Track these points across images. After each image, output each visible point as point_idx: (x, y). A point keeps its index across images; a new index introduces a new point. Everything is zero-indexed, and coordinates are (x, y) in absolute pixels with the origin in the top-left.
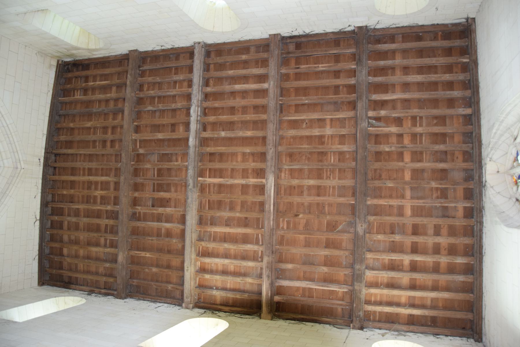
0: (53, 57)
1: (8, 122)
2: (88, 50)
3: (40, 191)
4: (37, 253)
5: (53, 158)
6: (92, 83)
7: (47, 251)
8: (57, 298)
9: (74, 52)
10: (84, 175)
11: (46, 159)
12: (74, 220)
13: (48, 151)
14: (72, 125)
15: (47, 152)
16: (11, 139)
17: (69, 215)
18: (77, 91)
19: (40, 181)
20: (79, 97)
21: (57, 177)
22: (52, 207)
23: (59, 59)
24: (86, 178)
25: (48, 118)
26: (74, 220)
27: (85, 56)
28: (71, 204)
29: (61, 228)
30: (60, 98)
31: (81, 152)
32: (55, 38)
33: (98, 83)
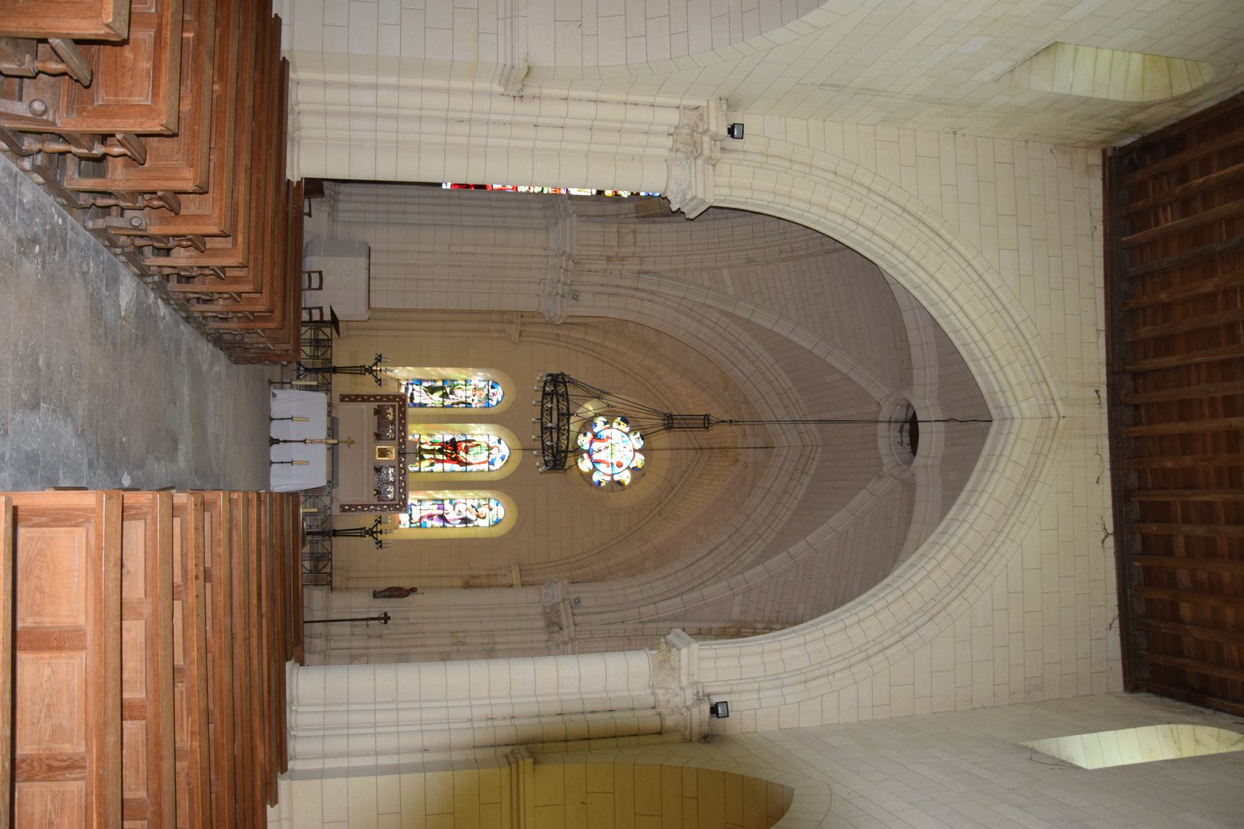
0: (1089, 146)
1: (1017, 318)
2: (1174, 99)
3: (1107, 465)
4: (1117, 612)
5: (1129, 383)
6: (1200, 181)
7: (1140, 609)
8: (1173, 726)
9: (1138, 117)
10: (1214, 416)
11: (1112, 388)
12: (1200, 531)
13: (1116, 369)
14: (1163, 296)
15: (1111, 373)
16: (1029, 354)
17: (1186, 521)
18: (1165, 210)
19: (1106, 443)
20: (1170, 224)
21: (1143, 430)
22: (1141, 502)
23: (1104, 146)
24: (1222, 423)
25: (1103, 291)
26: (1200, 531)
27: (1169, 118)
28: (1189, 492)
29: (1169, 551)
30: (1124, 239)
31: (1198, 360)
32: (1085, 101)
33: (1215, 175)
